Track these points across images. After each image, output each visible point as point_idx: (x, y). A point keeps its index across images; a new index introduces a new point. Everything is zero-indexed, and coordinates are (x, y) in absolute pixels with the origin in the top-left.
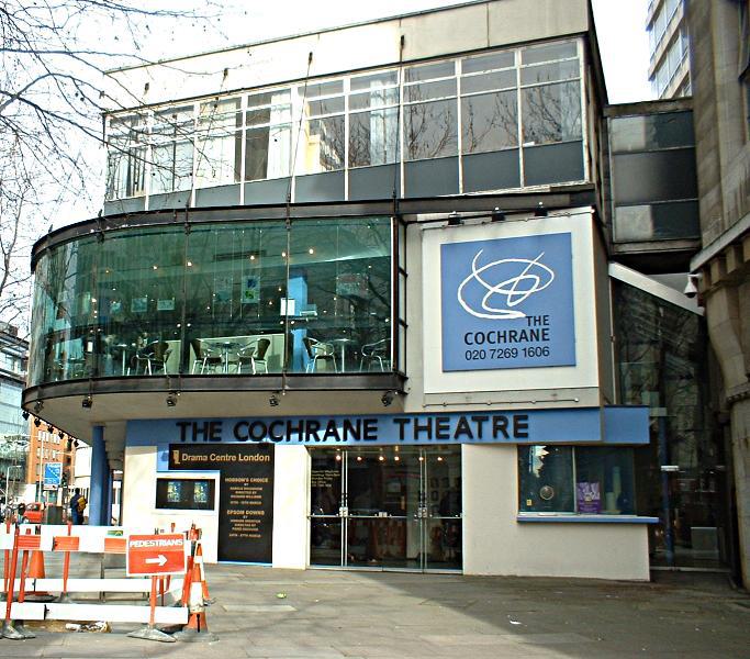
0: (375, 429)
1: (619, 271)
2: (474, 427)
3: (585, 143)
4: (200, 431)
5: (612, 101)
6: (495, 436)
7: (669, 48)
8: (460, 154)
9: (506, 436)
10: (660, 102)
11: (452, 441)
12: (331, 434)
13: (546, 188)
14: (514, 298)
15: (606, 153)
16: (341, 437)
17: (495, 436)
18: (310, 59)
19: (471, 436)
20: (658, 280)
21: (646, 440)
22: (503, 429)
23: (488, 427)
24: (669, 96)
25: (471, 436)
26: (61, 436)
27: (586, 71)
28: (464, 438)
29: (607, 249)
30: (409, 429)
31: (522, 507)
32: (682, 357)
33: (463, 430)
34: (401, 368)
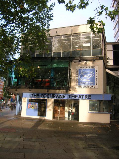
0: (90, 97)
1: (108, 71)
2: (82, 96)
3: (102, 49)
4: (35, 96)
5: (107, 42)
6: (85, 98)
7: (116, 35)
8: (81, 50)
9: (87, 98)
10: (115, 42)
11: (78, 99)
12: (80, 97)
13: (95, 56)
14: (88, 78)
15: (106, 50)
16: (82, 98)
17: (85, 98)
18: (56, 33)
19: (81, 98)
20: (114, 72)
21: (110, 99)
22: (87, 97)
23: (84, 97)
24: (116, 42)
25: (81, 98)
26: (14, 95)
27: (102, 37)
28: (80, 98)
29: (105, 66)
30: (71, 96)
31: (89, 110)
32: (81, 96)
33: (80, 97)
34: (70, 86)
